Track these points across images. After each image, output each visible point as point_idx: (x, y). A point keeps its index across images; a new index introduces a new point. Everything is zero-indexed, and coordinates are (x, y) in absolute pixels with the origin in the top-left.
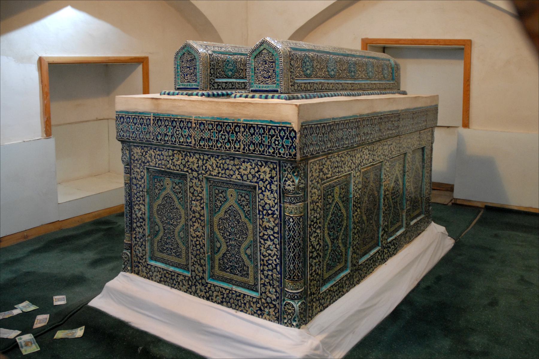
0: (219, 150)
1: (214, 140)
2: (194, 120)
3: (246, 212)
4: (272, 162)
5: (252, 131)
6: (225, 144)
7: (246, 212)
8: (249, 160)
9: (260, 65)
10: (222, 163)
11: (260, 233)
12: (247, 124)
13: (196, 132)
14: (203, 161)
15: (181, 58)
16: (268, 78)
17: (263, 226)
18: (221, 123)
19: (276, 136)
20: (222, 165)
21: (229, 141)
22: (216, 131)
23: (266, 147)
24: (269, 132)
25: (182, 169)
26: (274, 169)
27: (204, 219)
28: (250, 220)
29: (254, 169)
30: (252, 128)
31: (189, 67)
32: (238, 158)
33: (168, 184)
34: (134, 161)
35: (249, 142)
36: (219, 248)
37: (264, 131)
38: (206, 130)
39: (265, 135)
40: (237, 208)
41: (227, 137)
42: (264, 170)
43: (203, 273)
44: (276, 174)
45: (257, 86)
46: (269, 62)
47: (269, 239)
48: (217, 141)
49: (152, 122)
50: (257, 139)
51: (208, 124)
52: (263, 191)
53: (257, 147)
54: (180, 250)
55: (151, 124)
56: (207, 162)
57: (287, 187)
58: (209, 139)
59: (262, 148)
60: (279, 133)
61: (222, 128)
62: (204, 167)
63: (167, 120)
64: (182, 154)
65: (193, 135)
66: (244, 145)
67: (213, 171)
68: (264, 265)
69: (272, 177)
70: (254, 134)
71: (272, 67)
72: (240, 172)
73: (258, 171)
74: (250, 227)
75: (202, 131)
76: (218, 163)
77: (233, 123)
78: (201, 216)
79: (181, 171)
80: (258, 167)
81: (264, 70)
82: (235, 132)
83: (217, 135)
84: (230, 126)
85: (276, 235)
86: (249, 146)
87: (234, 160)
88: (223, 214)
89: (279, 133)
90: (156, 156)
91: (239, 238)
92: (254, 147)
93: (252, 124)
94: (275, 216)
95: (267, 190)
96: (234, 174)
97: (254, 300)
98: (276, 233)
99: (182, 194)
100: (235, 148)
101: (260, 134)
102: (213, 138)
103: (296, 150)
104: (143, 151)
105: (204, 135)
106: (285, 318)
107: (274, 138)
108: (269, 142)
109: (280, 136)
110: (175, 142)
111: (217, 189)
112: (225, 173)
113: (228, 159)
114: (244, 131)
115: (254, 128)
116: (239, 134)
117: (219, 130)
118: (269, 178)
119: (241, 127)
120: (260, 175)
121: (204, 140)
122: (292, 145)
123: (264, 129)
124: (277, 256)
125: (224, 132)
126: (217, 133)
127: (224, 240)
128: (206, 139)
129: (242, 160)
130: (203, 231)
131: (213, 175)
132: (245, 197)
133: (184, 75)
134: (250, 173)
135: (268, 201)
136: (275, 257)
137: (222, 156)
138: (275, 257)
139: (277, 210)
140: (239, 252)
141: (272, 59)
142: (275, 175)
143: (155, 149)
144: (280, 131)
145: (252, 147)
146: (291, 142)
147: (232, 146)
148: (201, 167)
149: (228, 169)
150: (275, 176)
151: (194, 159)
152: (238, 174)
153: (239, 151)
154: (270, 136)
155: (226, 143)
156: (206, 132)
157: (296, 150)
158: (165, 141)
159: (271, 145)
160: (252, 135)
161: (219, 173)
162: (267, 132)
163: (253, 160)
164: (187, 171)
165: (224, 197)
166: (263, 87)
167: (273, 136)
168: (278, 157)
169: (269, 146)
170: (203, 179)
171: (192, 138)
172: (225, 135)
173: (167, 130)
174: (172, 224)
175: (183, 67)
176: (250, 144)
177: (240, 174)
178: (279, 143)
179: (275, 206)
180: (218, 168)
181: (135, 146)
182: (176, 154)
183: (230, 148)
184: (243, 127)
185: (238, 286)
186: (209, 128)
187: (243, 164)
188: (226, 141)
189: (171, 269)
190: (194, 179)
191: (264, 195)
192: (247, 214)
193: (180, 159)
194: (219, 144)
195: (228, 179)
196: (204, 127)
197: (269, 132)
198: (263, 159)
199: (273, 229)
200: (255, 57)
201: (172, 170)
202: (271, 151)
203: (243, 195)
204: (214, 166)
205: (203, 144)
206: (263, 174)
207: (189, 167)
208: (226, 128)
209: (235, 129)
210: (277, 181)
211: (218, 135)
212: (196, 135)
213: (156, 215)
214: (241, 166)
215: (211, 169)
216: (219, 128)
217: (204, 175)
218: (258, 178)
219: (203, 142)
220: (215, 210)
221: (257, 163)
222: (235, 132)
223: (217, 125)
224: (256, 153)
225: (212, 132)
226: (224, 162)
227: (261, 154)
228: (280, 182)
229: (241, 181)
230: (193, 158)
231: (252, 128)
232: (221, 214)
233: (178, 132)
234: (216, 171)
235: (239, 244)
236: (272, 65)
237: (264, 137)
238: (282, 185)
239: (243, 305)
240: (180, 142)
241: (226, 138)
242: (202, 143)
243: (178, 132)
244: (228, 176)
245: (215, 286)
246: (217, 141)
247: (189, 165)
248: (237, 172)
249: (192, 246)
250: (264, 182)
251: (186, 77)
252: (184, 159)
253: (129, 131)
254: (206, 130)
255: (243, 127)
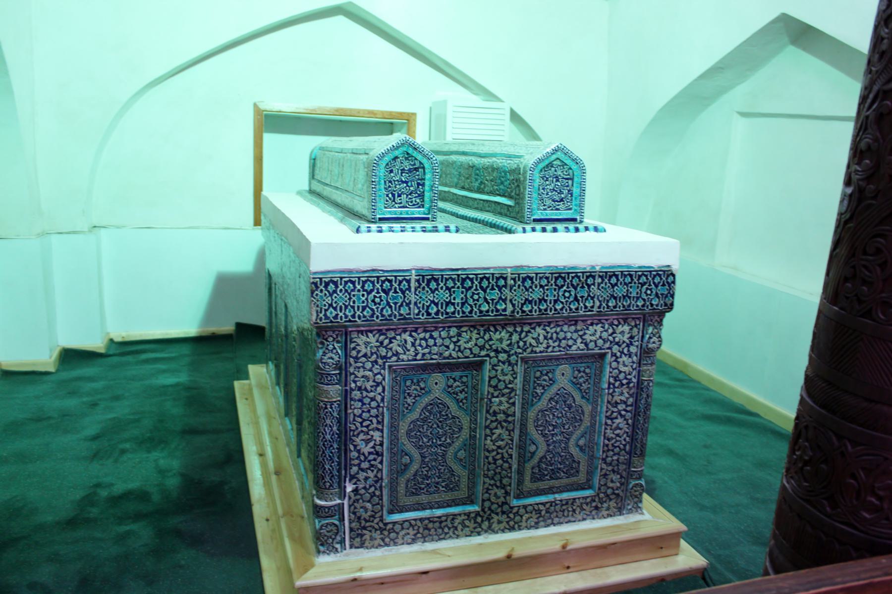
0: (559, 313)
1: (551, 300)
2: (512, 274)
3: (583, 391)
4: (633, 318)
5: (614, 280)
6: (570, 304)
7: (583, 391)
8: (600, 320)
9: (547, 182)
10: (556, 332)
11: (607, 412)
12: (606, 272)
13: (515, 293)
14: (520, 335)
15: (387, 164)
16: (560, 202)
17: (613, 401)
18: (563, 275)
19: (648, 284)
20: (555, 335)
21: (576, 299)
22: (554, 287)
23: (633, 300)
24: (639, 279)
25: (475, 354)
26: (636, 326)
27: (514, 420)
28: (588, 400)
29: (606, 331)
30: (485, 280)
31: (406, 182)
32: (583, 321)
33: (436, 384)
34: (356, 359)
35: (608, 296)
36: (533, 454)
37: (632, 279)
38: (536, 287)
39: (633, 285)
40: (570, 388)
41: (573, 293)
42: (622, 330)
43: (505, 497)
44: (639, 332)
45: (541, 213)
46: (563, 178)
47: (619, 416)
48: (556, 301)
49: (413, 284)
50: (620, 291)
51: (541, 278)
52: (617, 358)
53: (620, 302)
54: (457, 478)
55: (413, 289)
56: (529, 334)
57: (650, 346)
58: (540, 300)
59: (626, 301)
60: (653, 279)
61: (565, 281)
62: (521, 344)
63: (451, 278)
64: (478, 330)
65: (509, 298)
66: (600, 301)
67: (537, 346)
68: (608, 450)
69: (632, 337)
70: (335, 292)
71: (568, 186)
72: (584, 339)
73: (614, 332)
74: (587, 408)
75: (527, 290)
76: (548, 333)
77: (583, 273)
78: (508, 416)
79: (474, 357)
80: (613, 328)
81: (554, 190)
82: (587, 284)
83: (555, 293)
84: (579, 277)
85: (629, 409)
86: (608, 301)
87: (575, 324)
88: (546, 402)
89: (653, 279)
90: (418, 342)
91: (569, 428)
92: (616, 302)
93: (614, 272)
94: (631, 385)
95: (623, 355)
96: (574, 344)
97: (588, 500)
98: (629, 406)
99: (466, 393)
100: (586, 307)
101: (625, 284)
102: (549, 298)
103: (506, 304)
104: (382, 337)
105: (531, 295)
106: (628, 505)
107: (645, 287)
108: (637, 293)
109: (654, 283)
110: (353, 316)
111: (538, 371)
112: (559, 346)
113: (566, 324)
114: (602, 283)
115: (617, 276)
116: (592, 287)
117: (559, 285)
118: (628, 339)
119: (597, 277)
120: (614, 338)
121: (530, 302)
122: (404, 301)
123: (631, 276)
124: (627, 433)
125: (568, 287)
126: (555, 290)
127: (543, 439)
128: (536, 301)
129: (589, 322)
130: (510, 437)
131: (538, 351)
132: (584, 372)
133: (393, 195)
134: (600, 337)
135: (622, 369)
136: (625, 435)
137: (557, 321)
138: (625, 435)
139: (635, 377)
140: (566, 448)
141: (569, 175)
142: (637, 333)
143: (416, 331)
144: (655, 276)
145: (612, 302)
146: (401, 298)
147: (582, 305)
148: (516, 344)
149: (564, 339)
150: (636, 335)
151: (503, 334)
152: (582, 343)
153: (592, 311)
154: (640, 285)
155: (572, 301)
156: (536, 290)
157: (506, 304)
158: (447, 313)
159: (466, 301)
160: (613, 286)
161: (548, 347)
162: (635, 280)
163: (607, 320)
164: (487, 355)
165: (550, 380)
166: (551, 214)
167: (643, 284)
168: (650, 310)
169: (638, 298)
170: (517, 361)
171: (508, 302)
172: (569, 292)
173: (451, 295)
174: (440, 445)
175: (390, 182)
176: (610, 299)
177: (584, 341)
178: (652, 292)
179: (632, 372)
180: (547, 340)
181: (358, 332)
182: (466, 332)
183: (577, 309)
184: (600, 276)
185: (561, 492)
186: (626, 281)
187: (590, 327)
188: (571, 299)
189: (439, 512)
190: (500, 364)
191: (618, 363)
192: (584, 394)
193: (474, 339)
194: (559, 305)
195: (562, 353)
196: (532, 283)
197: (639, 279)
198: (621, 317)
199: (625, 403)
200: (541, 171)
201: (454, 358)
202: (640, 303)
203: (582, 369)
204: (541, 338)
205: (530, 308)
206: (619, 335)
207: (492, 348)
208: (571, 281)
209: (586, 280)
210: (638, 341)
211: (558, 293)
212: (516, 298)
213: (404, 440)
214: (587, 331)
215: (535, 344)
216: (560, 282)
217: (520, 356)
218: (611, 342)
219: (530, 306)
220: (533, 400)
221: (612, 322)
222: (587, 284)
223: (556, 279)
224: (618, 309)
225: (547, 290)
226: (558, 329)
227: (626, 310)
228: (642, 341)
229: (585, 351)
230: (500, 333)
231: (485, 280)
232: (543, 404)
233: (476, 297)
234: (545, 345)
235: (568, 437)
236: (567, 182)
237: (631, 287)
238: (644, 345)
239: (571, 513)
240: (481, 312)
241: (571, 295)
242: (527, 307)
243: (476, 297)
244: (564, 348)
245: (525, 507)
246: (556, 301)
247: (490, 346)
248: (579, 340)
249: (487, 464)
250: (620, 346)
251: (397, 200)
252: (483, 338)
253: (353, 307)
254: (536, 287)
255: (600, 276)
